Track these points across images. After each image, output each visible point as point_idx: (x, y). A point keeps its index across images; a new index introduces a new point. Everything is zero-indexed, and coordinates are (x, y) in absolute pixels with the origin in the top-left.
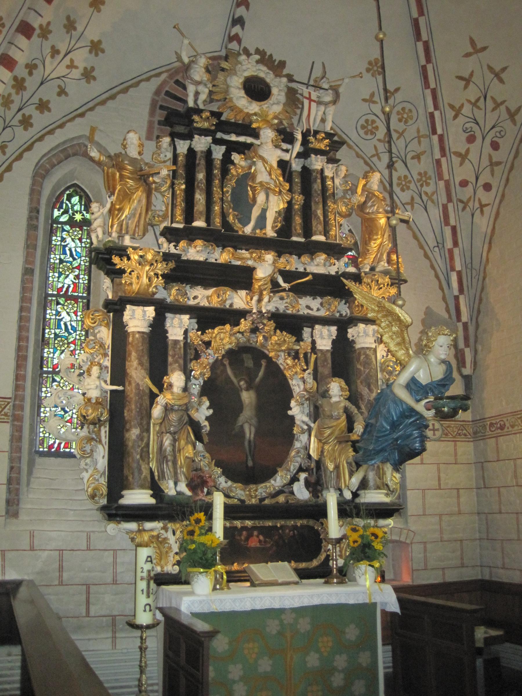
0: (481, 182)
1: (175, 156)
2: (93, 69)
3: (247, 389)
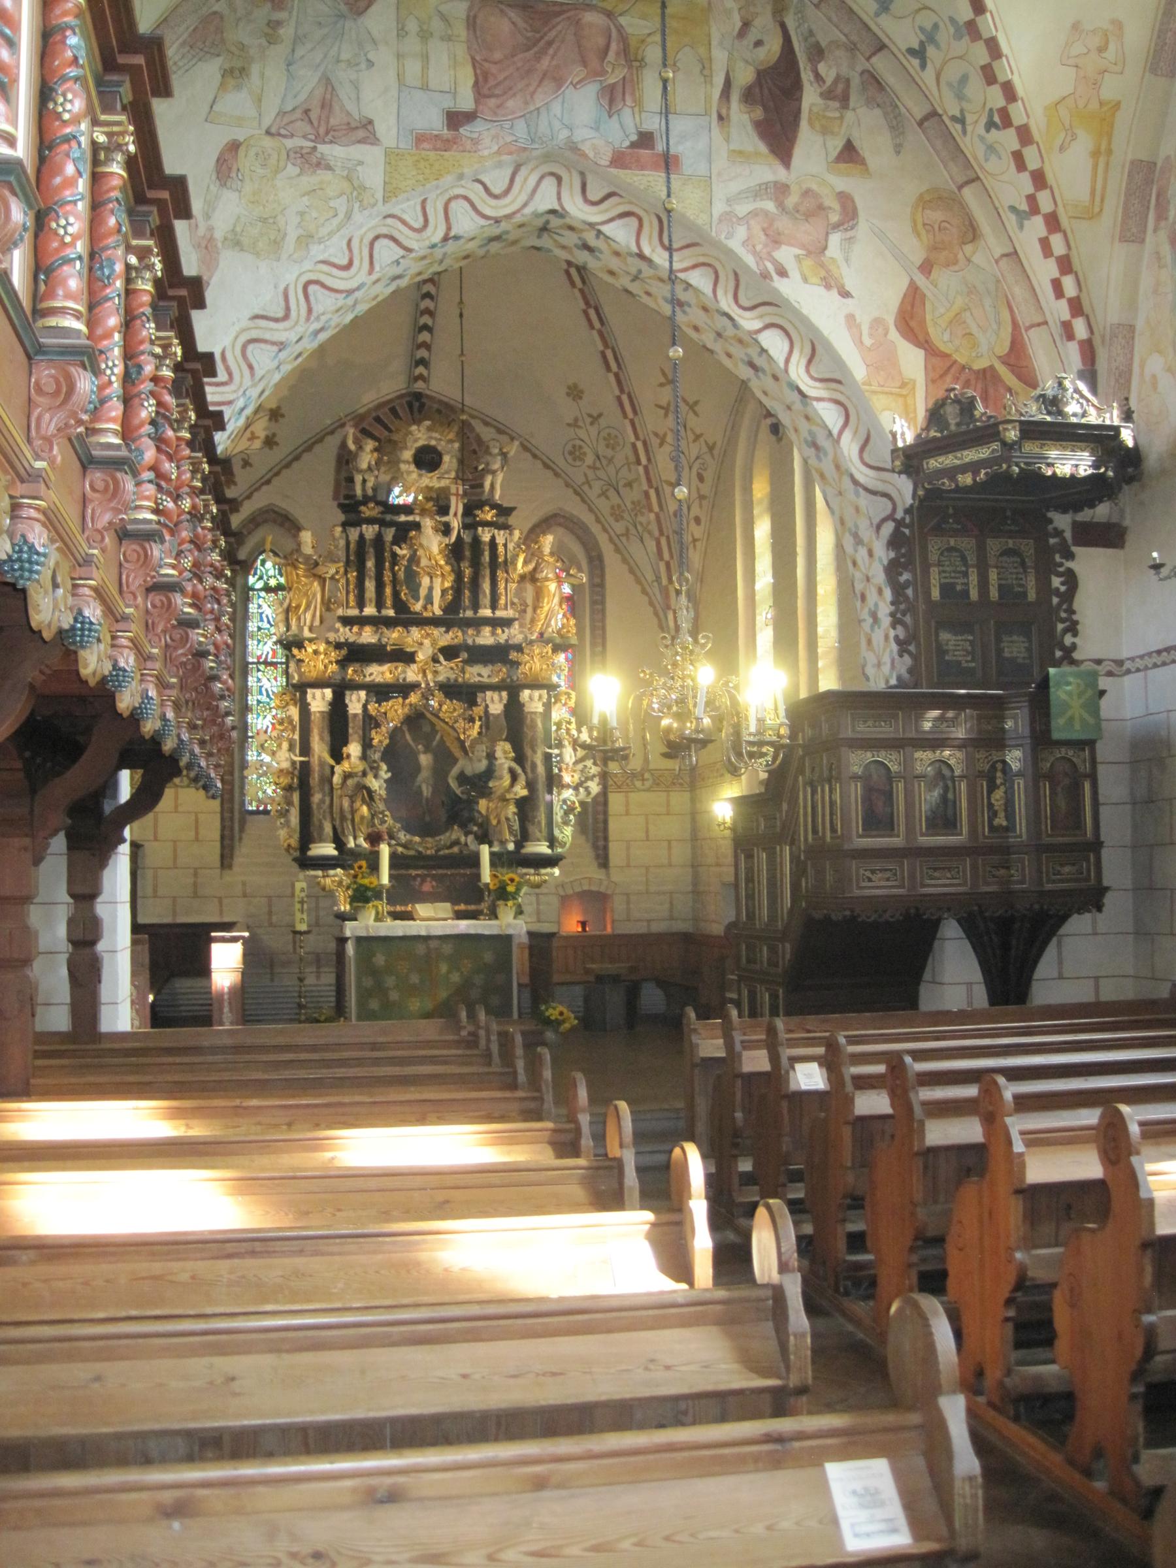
0: (692, 515)
1: (348, 543)
2: (274, 435)
3: (425, 752)
